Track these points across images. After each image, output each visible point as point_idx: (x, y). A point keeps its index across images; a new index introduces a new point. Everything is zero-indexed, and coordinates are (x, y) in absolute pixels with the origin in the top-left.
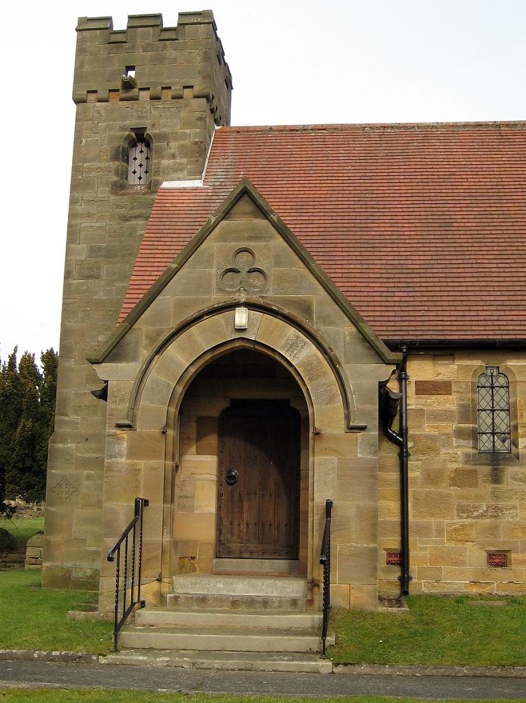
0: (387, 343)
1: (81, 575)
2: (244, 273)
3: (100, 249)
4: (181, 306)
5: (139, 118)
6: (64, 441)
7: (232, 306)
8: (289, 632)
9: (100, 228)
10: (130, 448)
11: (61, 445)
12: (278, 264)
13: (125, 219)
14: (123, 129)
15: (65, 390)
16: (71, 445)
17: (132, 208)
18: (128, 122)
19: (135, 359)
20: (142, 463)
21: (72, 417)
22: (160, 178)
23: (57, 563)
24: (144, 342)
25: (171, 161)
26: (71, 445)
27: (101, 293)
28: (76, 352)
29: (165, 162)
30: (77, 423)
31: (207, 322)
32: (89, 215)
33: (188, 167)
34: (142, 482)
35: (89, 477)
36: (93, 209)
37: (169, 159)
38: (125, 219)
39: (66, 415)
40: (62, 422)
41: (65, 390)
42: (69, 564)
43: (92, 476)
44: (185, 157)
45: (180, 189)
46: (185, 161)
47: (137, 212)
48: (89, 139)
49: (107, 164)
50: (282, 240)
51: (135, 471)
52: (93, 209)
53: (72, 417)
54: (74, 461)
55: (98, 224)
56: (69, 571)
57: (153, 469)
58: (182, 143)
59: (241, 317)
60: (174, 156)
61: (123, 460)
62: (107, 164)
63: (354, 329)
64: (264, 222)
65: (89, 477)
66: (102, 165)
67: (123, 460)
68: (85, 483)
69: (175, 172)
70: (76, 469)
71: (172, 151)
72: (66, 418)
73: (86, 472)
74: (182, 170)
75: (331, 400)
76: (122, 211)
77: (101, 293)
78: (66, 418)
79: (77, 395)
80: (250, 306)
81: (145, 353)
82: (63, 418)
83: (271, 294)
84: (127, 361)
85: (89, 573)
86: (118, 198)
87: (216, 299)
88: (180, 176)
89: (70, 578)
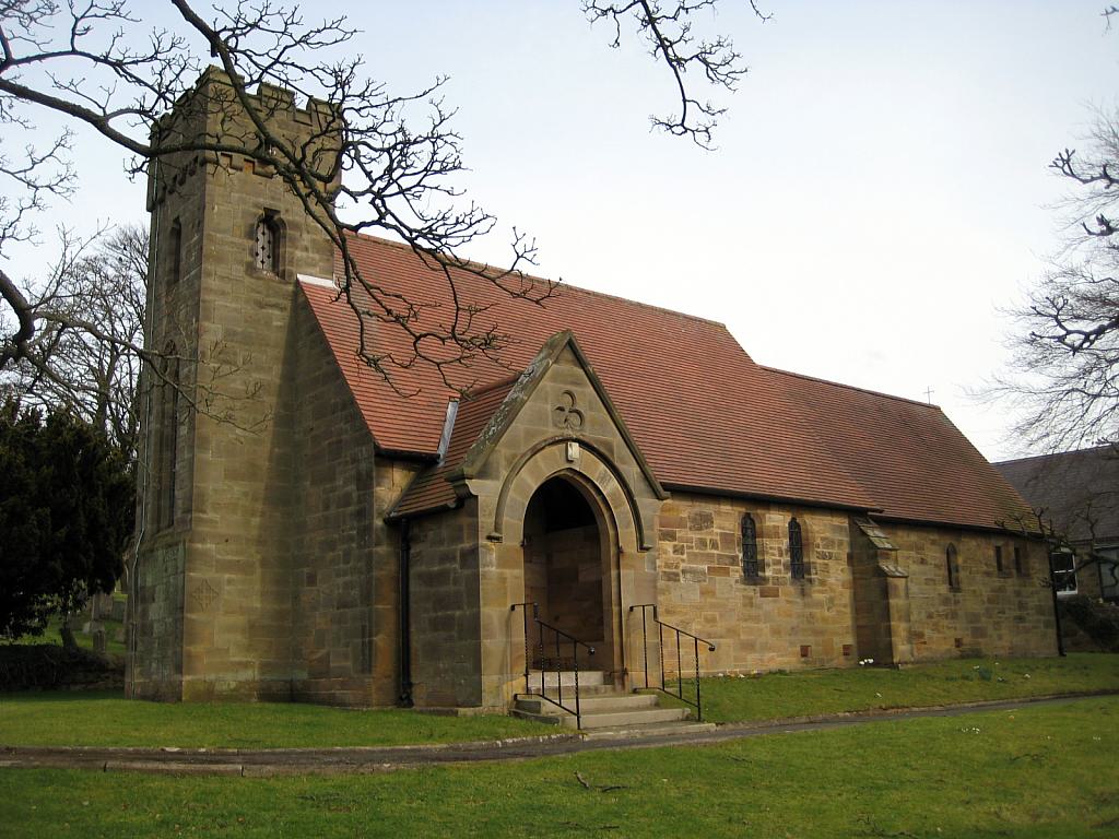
0: (662, 484)
1: (225, 687)
2: (567, 410)
3: (235, 333)
4: (529, 434)
5: (273, 198)
6: (203, 541)
7: (566, 440)
8: (638, 708)
9: (236, 310)
10: (499, 558)
11: (199, 546)
12: (591, 409)
13: (261, 305)
14: (256, 206)
15: (202, 485)
16: (210, 546)
17: (267, 296)
18: (262, 200)
19: (497, 478)
20: (508, 572)
21: (210, 515)
22: (294, 269)
23: (201, 677)
24: (503, 463)
25: (304, 254)
26: (210, 546)
27: (238, 382)
28: (213, 444)
29: (299, 254)
30: (217, 522)
31: (548, 449)
32: (223, 293)
33: (321, 264)
34: (509, 589)
35: (229, 582)
36: (228, 287)
37: (302, 251)
38: (261, 305)
39: (204, 512)
40: (201, 520)
41: (202, 485)
42: (212, 677)
43: (233, 580)
44: (318, 252)
45: (317, 286)
46: (317, 256)
47: (273, 300)
48: (221, 207)
49: (241, 241)
50: (592, 388)
51: (503, 580)
52: (228, 287)
53: (210, 515)
54: (214, 563)
55: (234, 305)
56: (211, 683)
57: (516, 578)
58: (314, 237)
59: (575, 450)
60: (307, 249)
61: (494, 569)
62: (241, 241)
63: (639, 470)
64: (581, 371)
65: (229, 582)
66: (236, 240)
67: (494, 569)
68: (227, 588)
69: (309, 266)
70: (217, 572)
71: (305, 243)
72: (205, 516)
73: (227, 576)
74: (314, 266)
75: (628, 526)
76: (258, 297)
77: (238, 382)
78: (205, 516)
79: (215, 491)
80: (583, 444)
81: (504, 473)
82: (201, 515)
83: (588, 435)
84: (492, 479)
85: (233, 685)
86: (253, 281)
87: (552, 432)
88: (313, 271)
89: (213, 692)
